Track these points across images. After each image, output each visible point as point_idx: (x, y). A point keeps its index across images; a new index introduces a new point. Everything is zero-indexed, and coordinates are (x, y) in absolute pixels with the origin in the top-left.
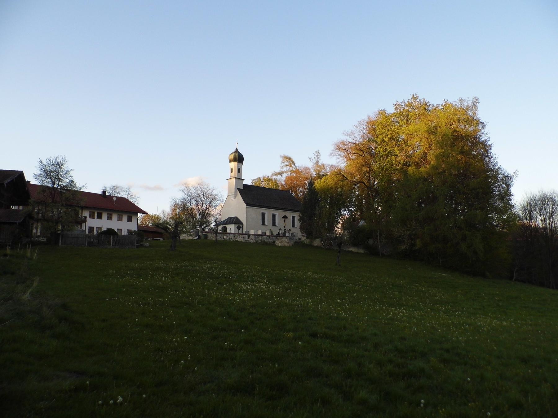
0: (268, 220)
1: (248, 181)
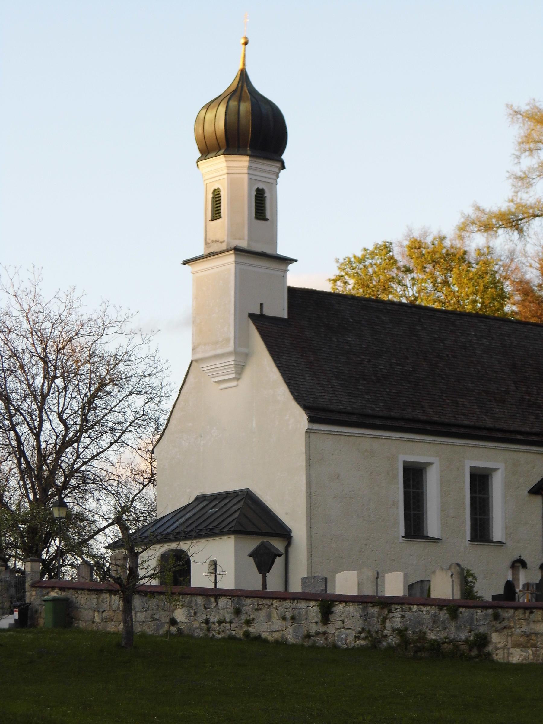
0: (443, 508)
1: (314, 270)
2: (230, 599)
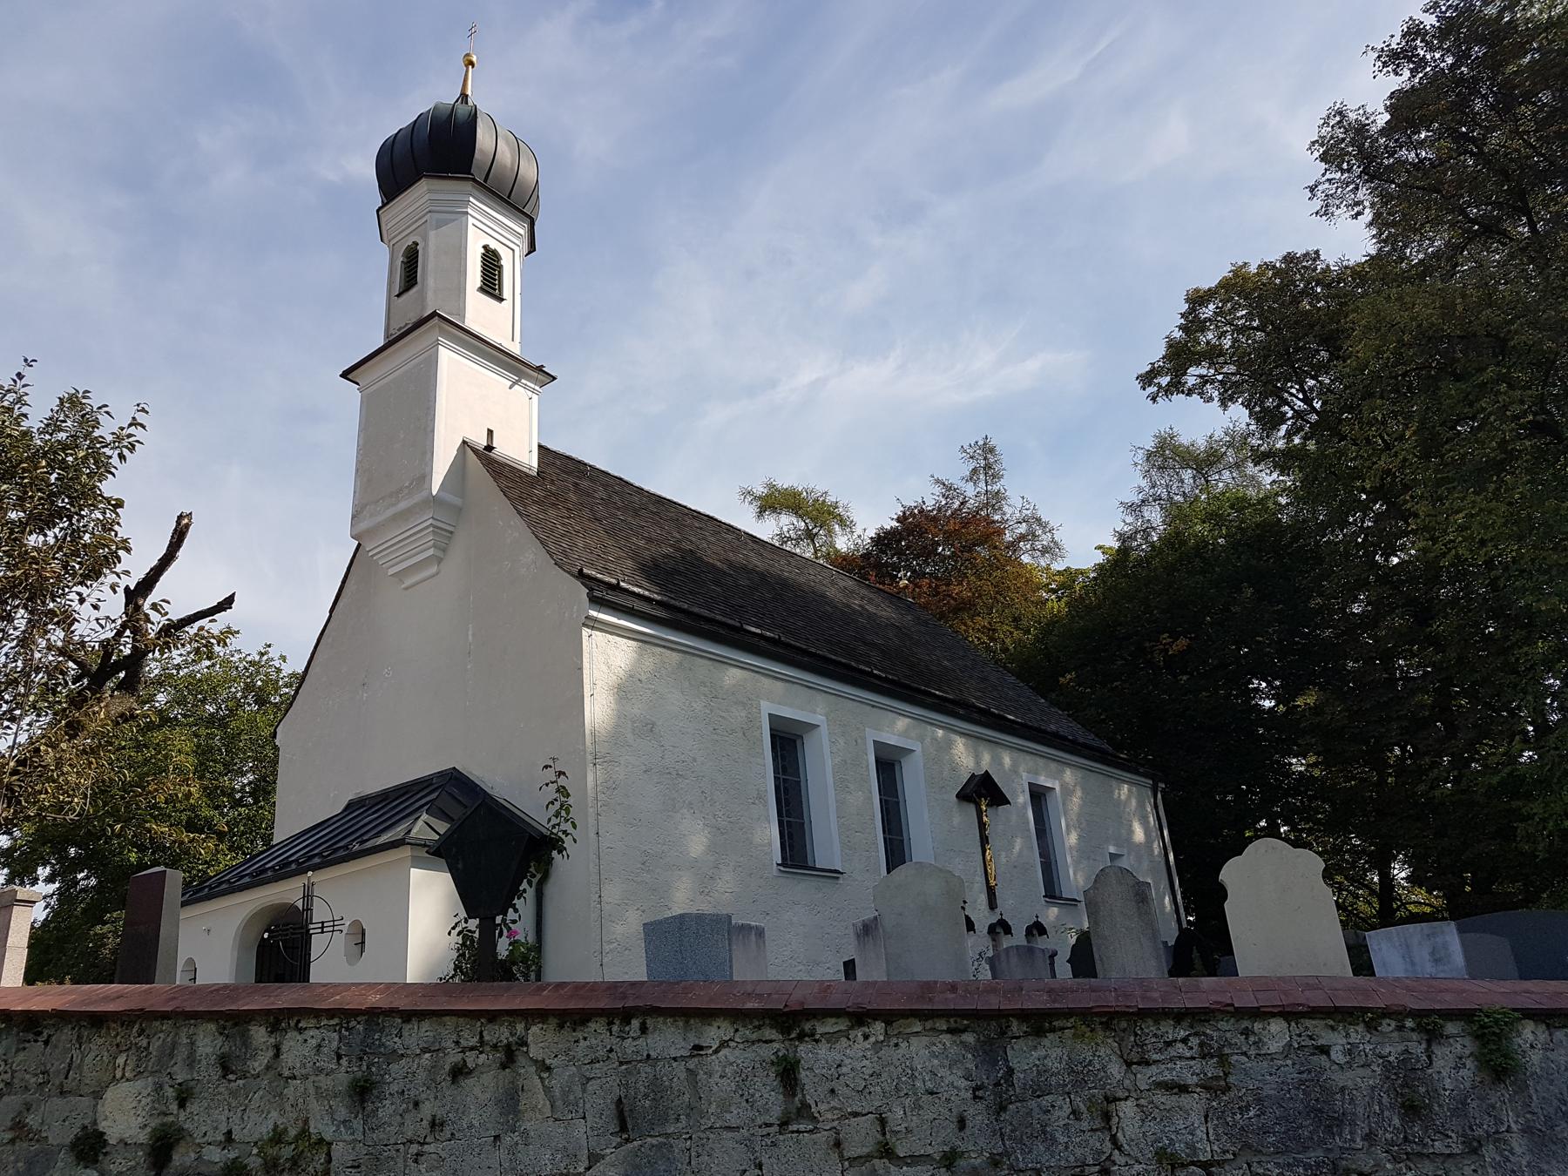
2: (333, 1028)
